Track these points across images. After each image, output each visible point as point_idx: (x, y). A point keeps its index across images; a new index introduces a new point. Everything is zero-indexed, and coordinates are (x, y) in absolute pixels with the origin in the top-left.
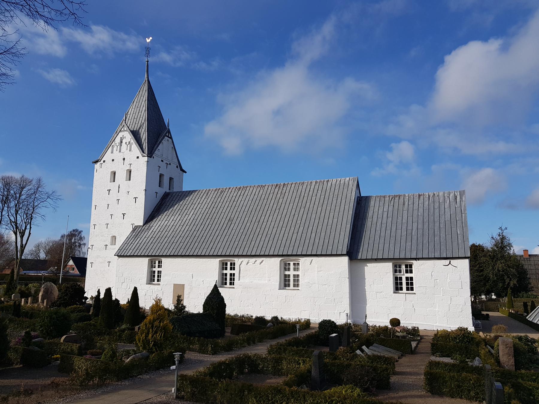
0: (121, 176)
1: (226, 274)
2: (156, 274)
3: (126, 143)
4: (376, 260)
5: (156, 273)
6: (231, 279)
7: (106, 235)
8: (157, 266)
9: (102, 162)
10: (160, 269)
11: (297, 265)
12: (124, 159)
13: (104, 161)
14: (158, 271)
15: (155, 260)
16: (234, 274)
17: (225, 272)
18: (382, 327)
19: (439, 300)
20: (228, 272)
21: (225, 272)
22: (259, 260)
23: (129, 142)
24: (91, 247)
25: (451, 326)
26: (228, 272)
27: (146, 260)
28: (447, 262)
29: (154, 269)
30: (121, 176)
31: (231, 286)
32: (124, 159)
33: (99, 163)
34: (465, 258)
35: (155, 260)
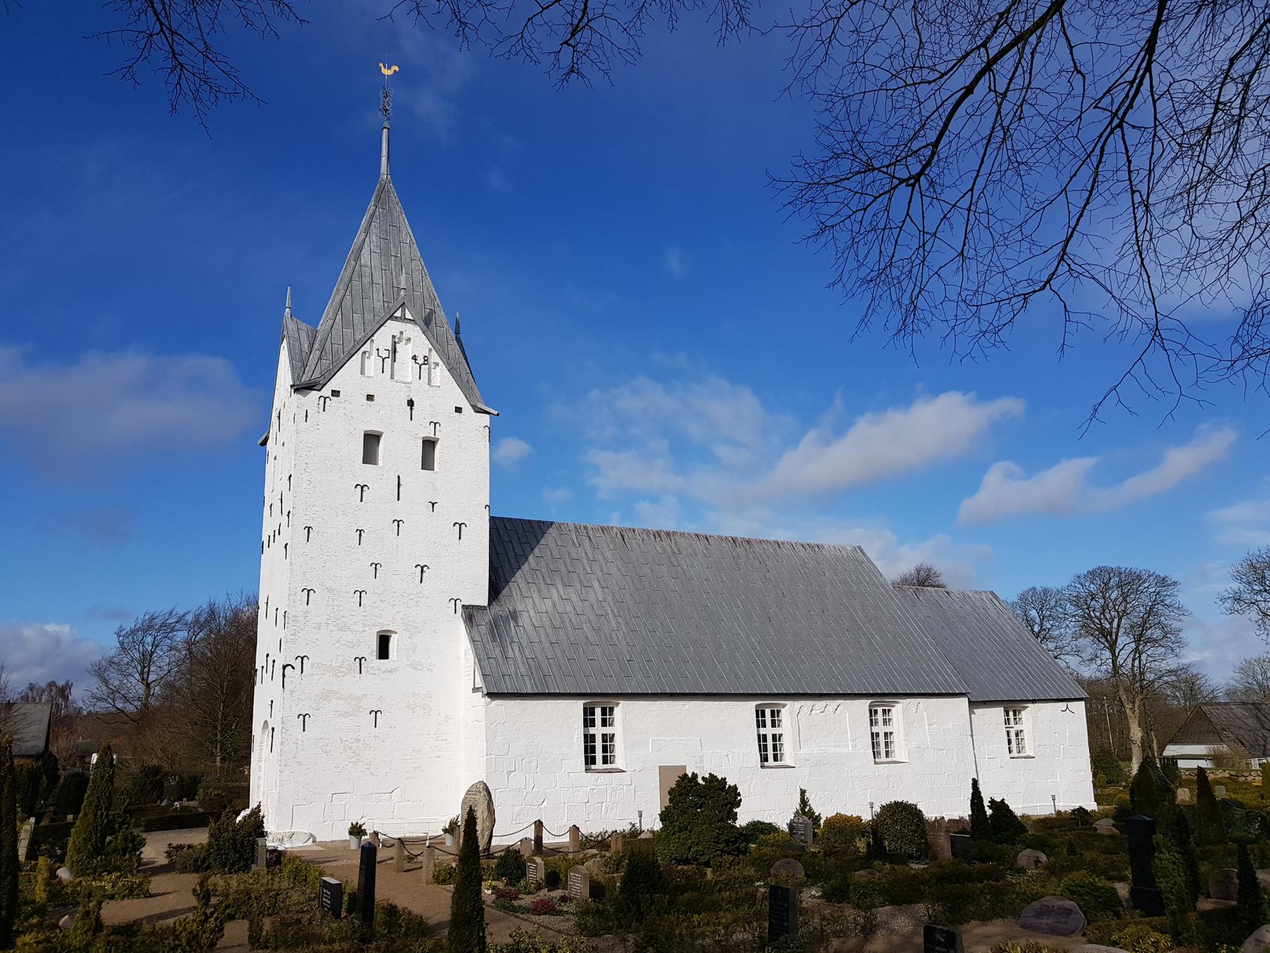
0: (399, 450)
1: (765, 736)
2: (882, 739)
3: (414, 358)
4: (1034, 701)
5: (770, 739)
6: (605, 749)
7: (360, 628)
8: (769, 723)
9: (326, 391)
10: (608, 730)
11: (785, 714)
12: (411, 403)
13: (336, 393)
14: (604, 735)
15: (598, 705)
16: (781, 735)
17: (762, 731)
18: (844, 827)
19: (1047, 767)
20: (769, 731)
21: (762, 731)
22: (833, 704)
23: (426, 359)
24: (297, 664)
25: (1067, 804)
26: (769, 731)
27: (578, 706)
28: (1063, 705)
29: (592, 731)
30: (399, 450)
31: (606, 766)
32: (411, 403)
33: (314, 394)
34: (1081, 699)
35: (598, 705)
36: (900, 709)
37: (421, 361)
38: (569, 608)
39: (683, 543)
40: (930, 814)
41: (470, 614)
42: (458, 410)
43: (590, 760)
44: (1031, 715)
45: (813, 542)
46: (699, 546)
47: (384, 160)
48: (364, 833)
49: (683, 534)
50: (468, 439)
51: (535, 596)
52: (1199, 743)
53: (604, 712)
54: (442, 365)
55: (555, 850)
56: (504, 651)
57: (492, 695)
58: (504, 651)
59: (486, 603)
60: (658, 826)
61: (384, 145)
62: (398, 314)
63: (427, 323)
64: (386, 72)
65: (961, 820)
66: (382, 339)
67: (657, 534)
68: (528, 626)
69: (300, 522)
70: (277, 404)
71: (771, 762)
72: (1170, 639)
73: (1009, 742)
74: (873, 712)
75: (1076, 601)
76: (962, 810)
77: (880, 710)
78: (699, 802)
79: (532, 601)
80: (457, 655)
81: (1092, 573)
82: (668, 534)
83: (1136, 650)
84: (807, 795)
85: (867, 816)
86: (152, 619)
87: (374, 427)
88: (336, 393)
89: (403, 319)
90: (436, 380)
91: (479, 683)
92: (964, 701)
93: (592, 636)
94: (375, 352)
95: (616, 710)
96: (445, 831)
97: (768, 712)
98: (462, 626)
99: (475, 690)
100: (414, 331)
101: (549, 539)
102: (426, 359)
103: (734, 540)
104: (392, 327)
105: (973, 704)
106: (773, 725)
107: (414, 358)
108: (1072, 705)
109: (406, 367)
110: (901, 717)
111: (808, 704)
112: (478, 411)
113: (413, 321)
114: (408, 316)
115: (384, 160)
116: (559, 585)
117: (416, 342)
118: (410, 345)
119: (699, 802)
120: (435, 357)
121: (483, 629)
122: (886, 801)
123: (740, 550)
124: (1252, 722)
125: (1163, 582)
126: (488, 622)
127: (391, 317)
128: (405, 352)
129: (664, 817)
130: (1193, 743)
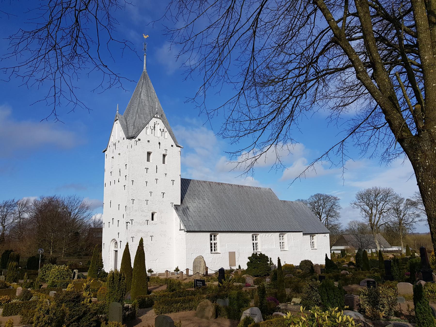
0: (156, 157)
3: (160, 130)
4: (317, 234)
9: (137, 139)
11: (258, 237)
12: (159, 143)
13: (139, 140)
18: (290, 268)
20: (213, 242)
21: (253, 242)
22: (271, 234)
23: (163, 130)
28: (324, 234)
32: (159, 143)
33: (133, 140)
36: (286, 235)
37: (162, 131)
38: (201, 206)
39: (226, 186)
40: (314, 263)
41: (176, 207)
42: (172, 146)
43: (212, 250)
44: (316, 237)
45: (259, 187)
46: (230, 187)
47: (145, 65)
48: (179, 271)
49: (225, 184)
50: (174, 154)
51: (192, 202)
52: (341, 246)
53: (214, 236)
54: (168, 133)
55: (210, 275)
56: (188, 219)
57: (188, 232)
58: (188, 219)
59: (180, 204)
60: (245, 267)
61: (145, 61)
62: (156, 116)
63: (161, 118)
64: (145, 37)
65: (321, 266)
66: (151, 123)
67: (219, 184)
68: (192, 211)
69: (130, 179)
70: (112, 140)
71: (213, 251)
72: (337, 215)
73: (254, 247)
74: (211, 236)
75: (310, 204)
76: (323, 262)
77: (281, 236)
78: (258, 261)
79: (193, 205)
80: (174, 219)
81: (316, 195)
82: (221, 183)
83: (327, 219)
84: (272, 259)
85: (298, 264)
86: (6, 203)
87: (149, 150)
88: (139, 140)
89: (157, 117)
90: (166, 137)
91: (182, 227)
92: (302, 233)
93: (209, 215)
94: (149, 127)
95: (217, 236)
96: (175, 271)
97: (254, 236)
98: (174, 211)
99: (180, 230)
100: (160, 121)
101: (191, 184)
102: (163, 130)
103: (238, 186)
104: (154, 120)
105: (304, 234)
106: (214, 240)
107: (160, 130)
108: (326, 234)
109: (158, 133)
110: (286, 238)
111: (265, 234)
112: (178, 146)
113: (160, 118)
114: (158, 117)
115: (145, 65)
116: (197, 199)
117: (160, 125)
118: (159, 125)
119: (258, 261)
120: (166, 130)
121: (181, 212)
122: (303, 259)
123: (241, 189)
124: (356, 240)
125: (335, 199)
126: (181, 209)
127: (154, 117)
128: (158, 127)
129: (248, 264)
130: (340, 246)
